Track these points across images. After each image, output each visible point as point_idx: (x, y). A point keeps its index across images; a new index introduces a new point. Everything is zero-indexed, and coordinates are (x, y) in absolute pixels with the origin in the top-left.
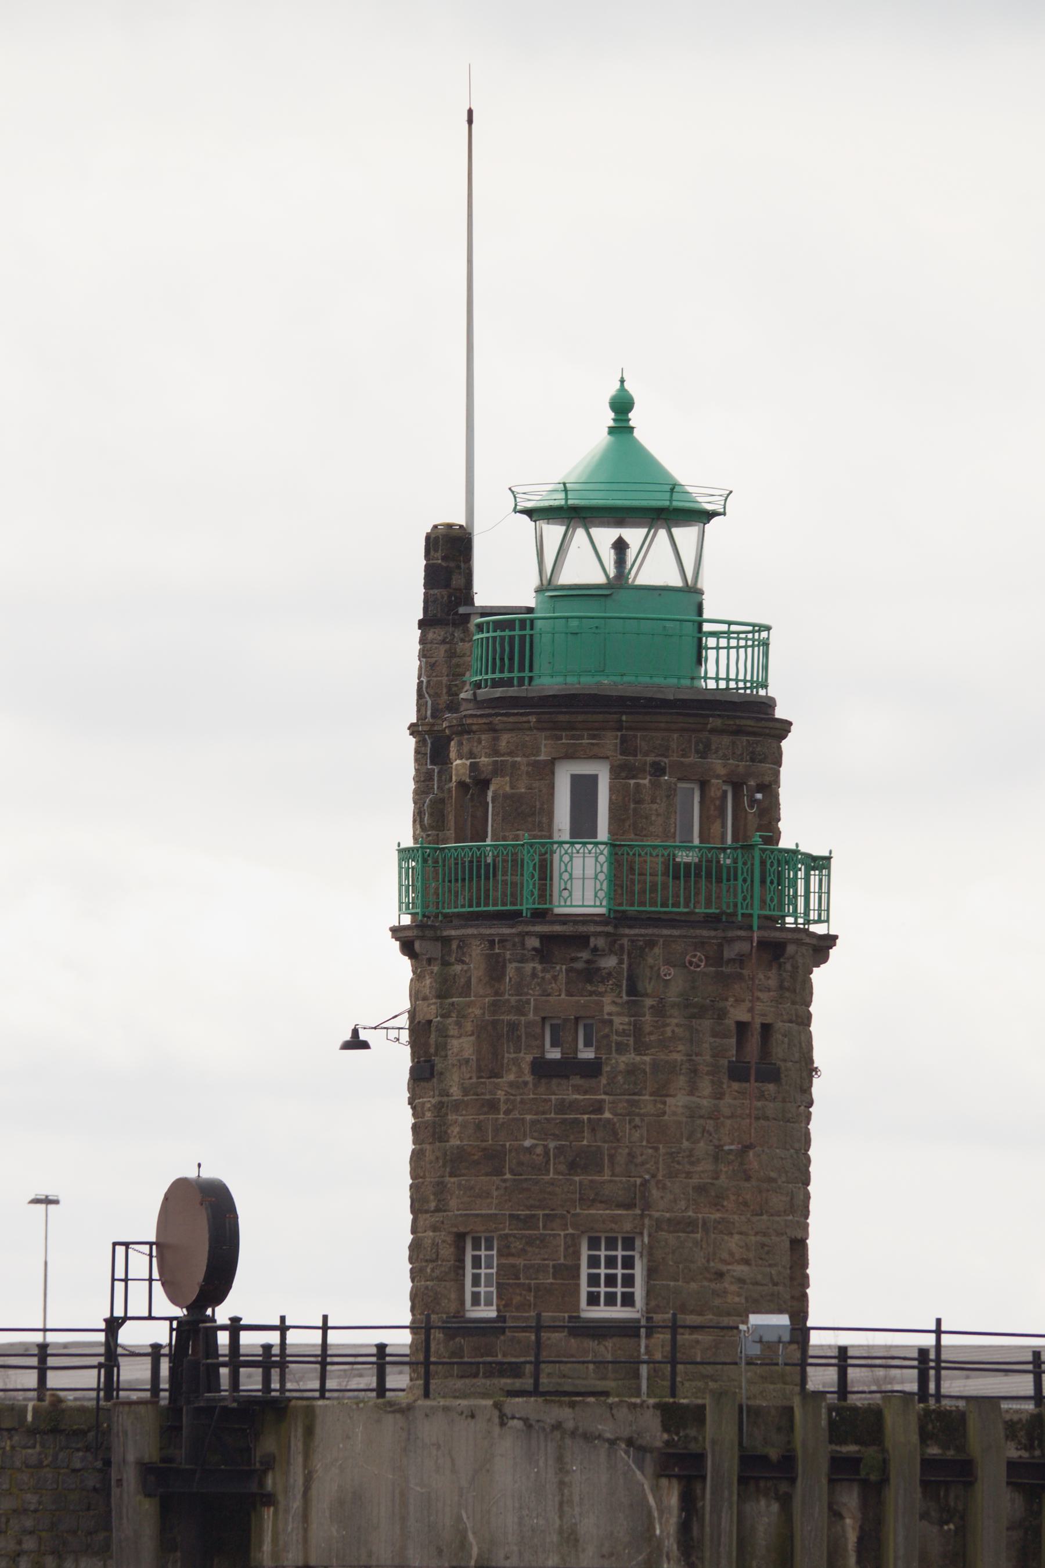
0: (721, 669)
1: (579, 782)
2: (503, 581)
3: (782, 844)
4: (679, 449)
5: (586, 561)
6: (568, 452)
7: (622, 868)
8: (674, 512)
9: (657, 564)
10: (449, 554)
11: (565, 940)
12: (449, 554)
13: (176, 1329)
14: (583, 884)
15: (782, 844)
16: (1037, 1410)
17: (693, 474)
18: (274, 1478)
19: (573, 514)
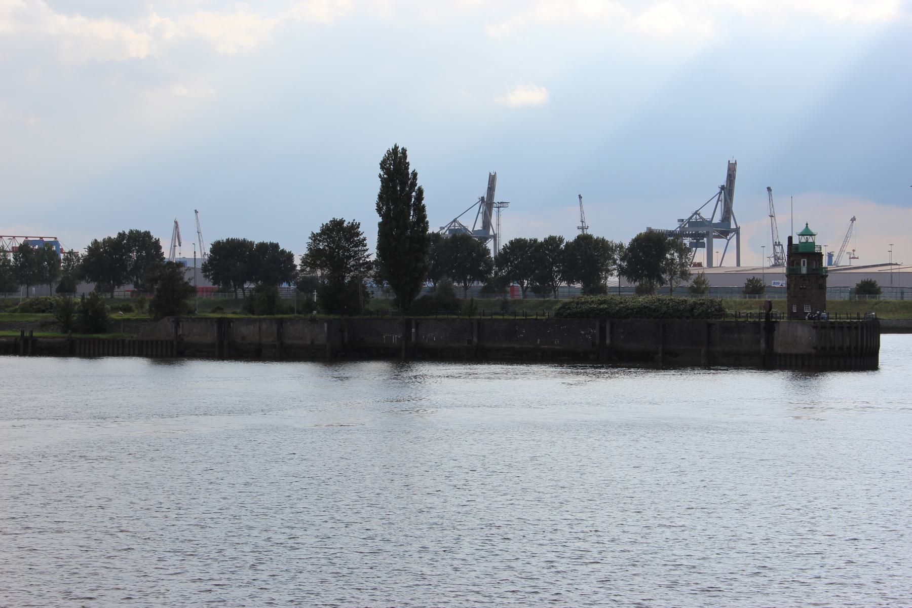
0: (817, 250)
1: (804, 261)
2: (795, 241)
3: (430, 231)
4: (812, 229)
5: (803, 240)
6: (801, 229)
7: (808, 269)
8: (812, 235)
9: (810, 240)
10: (790, 239)
11: (803, 276)
12: (790, 239)
13: (737, 322)
14: (804, 270)
15: (430, 231)
16: (202, 282)
17: (813, 231)
18: (115, 310)
19: (802, 235)
